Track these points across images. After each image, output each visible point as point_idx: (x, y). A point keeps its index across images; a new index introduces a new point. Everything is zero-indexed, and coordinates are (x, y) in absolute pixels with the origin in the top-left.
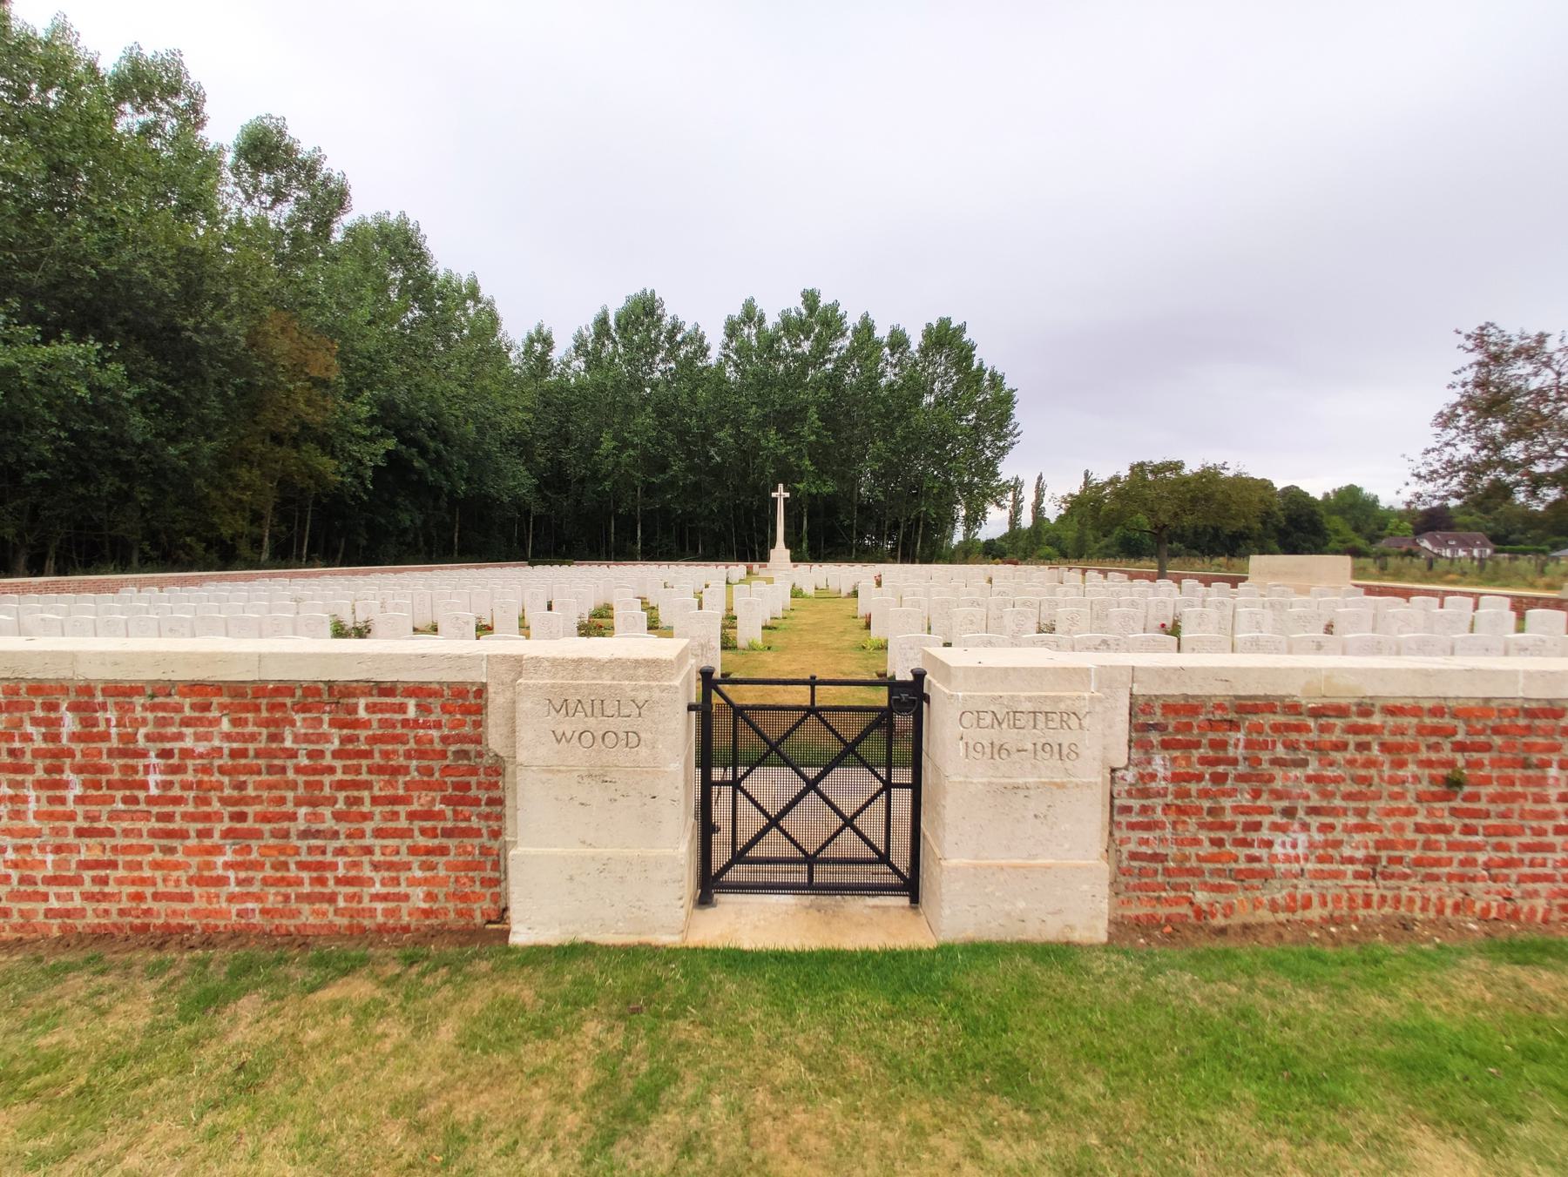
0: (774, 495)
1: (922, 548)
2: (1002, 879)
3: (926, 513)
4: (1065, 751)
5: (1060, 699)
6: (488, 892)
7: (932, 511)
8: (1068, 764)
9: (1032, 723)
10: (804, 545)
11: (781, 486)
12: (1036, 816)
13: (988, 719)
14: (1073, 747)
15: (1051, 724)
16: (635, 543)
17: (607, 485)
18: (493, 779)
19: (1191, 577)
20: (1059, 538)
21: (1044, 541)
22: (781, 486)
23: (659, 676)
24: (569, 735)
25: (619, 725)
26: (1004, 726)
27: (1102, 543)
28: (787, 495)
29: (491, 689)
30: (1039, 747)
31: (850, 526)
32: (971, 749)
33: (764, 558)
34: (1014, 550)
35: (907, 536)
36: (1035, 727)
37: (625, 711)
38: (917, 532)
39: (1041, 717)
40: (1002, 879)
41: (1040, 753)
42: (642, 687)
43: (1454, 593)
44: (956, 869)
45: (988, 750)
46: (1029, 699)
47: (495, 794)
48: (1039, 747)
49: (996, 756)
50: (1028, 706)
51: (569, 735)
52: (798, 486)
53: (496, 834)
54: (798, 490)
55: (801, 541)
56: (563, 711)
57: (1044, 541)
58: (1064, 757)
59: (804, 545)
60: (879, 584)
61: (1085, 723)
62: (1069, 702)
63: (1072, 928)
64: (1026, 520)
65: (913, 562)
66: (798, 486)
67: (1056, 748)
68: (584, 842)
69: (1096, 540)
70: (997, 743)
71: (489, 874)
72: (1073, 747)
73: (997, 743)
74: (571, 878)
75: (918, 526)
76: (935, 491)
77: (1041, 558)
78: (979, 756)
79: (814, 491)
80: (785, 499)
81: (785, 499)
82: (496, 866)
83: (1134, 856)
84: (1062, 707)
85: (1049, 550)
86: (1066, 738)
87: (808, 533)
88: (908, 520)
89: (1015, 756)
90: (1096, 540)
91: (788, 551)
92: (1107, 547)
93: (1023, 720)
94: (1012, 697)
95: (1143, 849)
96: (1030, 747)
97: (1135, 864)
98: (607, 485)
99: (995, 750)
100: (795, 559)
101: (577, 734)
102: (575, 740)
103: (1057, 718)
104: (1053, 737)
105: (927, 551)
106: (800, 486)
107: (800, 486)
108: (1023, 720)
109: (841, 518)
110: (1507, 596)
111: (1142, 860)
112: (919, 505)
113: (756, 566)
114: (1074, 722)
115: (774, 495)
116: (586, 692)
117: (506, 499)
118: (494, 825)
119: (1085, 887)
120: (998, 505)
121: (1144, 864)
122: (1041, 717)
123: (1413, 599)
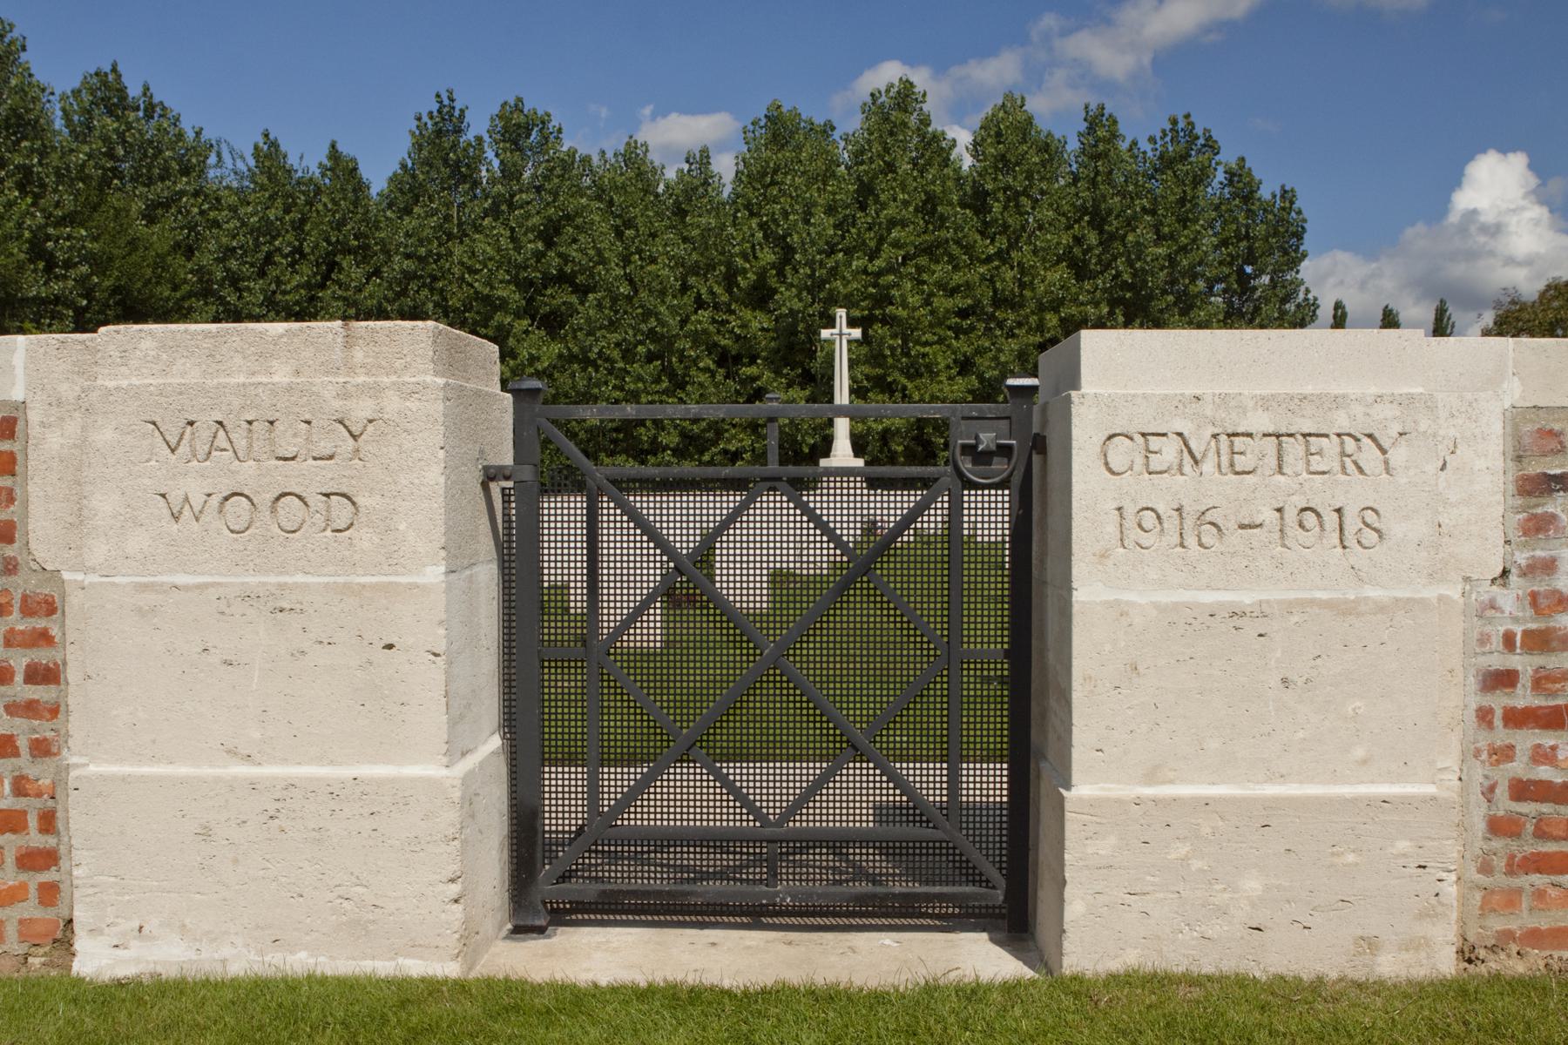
2: (1206, 830)
4: (1352, 524)
5: (1338, 401)
6: (34, 880)
8: (1357, 555)
9: (1272, 461)
12: (1284, 681)
13: (1169, 451)
14: (1370, 517)
15: (1317, 463)
18: (40, 623)
23: (398, 364)
24: (197, 500)
25: (310, 477)
26: (1208, 466)
29: (34, 416)
30: (1291, 515)
32: (1131, 522)
36: (1280, 470)
37: (325, 447)
39: (1294, 449)
40: (1206, 830)
41: (1293, 531)
42: (363, 389)
44: (1094, 804)
45: (1171, 524)
46: (1265, 403)
47: (43, 656)
48: (1291, 515)
49: (1191, 541)
50: (1260, 422)
51: (197, 500)
53: (42, 749)
56: (184, 449)
58: (1350, 540)
60: (1261, 635)
61: (1398, 456)
62: (1358, 410)
63: (1370, 944)
67: (1331, 519)
68: (232, 752)
70: (1191, 510)
71: (35, 839)
72: (1370, 517)
73: (1191, 510)
74: (205, 833)
78: (1146, 540)
82: (48, 822)
83: (1521, 790)
84: (1342, 422)
86: (1353, 494)
89: (1236, 538)
93: (1256, 453)
94: (1224, 398)
95: (1544, 773)
96: (1269, 516)
97: (1528, 808)
99: (1189, 523)
101: (215, 501)
102: (210, 516)
103: (1330, 446)
104: (1323, 495)
108: (1256, 453)
111: (1542, 800)
114: (1369, 456)
116: (236, 403)
118: (44, 729)
119: (1403, 845)
121: (1546, 808)
122: (1294, 449)
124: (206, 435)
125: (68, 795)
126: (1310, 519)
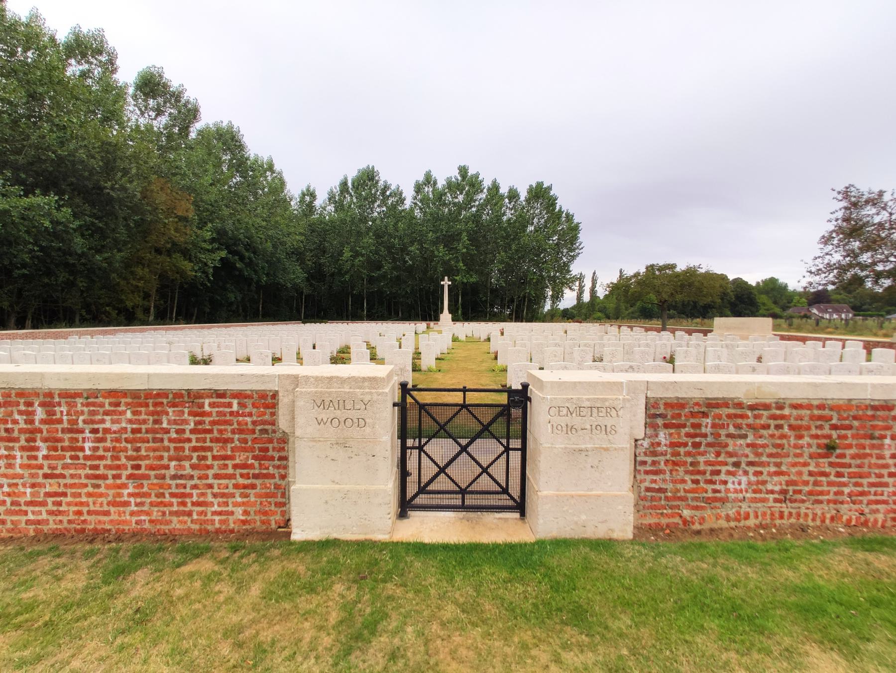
0: (442, 283)
1: (527, 313)
2: (572, 503)
3: (529, 293)
4: (609, 429)
5: (606, 400)
7: (532, 292)
8: (611, 437)
9: (590, 414)
10: (460, 312)
11: (446, 278)
12: (592, 467)
13: (565, 411)
14: (613, 427)
15: (601, 414)
16: (363, 311)
17: (347, 277)
18: (282, 446)
19: (681, 330)
20: (605, 308)
21: (597, 309)
22: (446, 278)
23: (377, 386)
24: (325, 420)
25: (354, 414)
26: (574, 415)
27: (630, 311)
28: (450, 283)
29: (280, 394)
30: (594, 427)
31: (486, 301)
32: (555, 428)
33: (437, 319)
34: (580, 315)
35: (518, 306)
36: (591, 416)
37: (357, 407)
38: (524, 304)
39: (595, 410)
40: (572, 503)
41: (594, 430)
42: (367, 393)
43: (831, 339)
45: (565, 429)
46: (588, 400)
47: (283, 454)
48: (594, 427)
49: (569, 432)
50: (587, 404)
51: (325, 420)
52: (456, 278)
53: (283, 477)
54: (456, 280)
55: (458, 309)
56: (322, 407)
57: (597, 309)
58: (608, 433)
59: (460, 312)
60: (502, 334)
61: (620, 413)
62: (611, 402)
63: (612, 530)
64: (586, 297)
65: (522, 321)
66: (456, 278)
67: (603, 428)
68: (333, 482)
69: (626, 309)
70: (570, 425)
71: (279, 500)
72: (613, 427)
73: (570, 425)
74: (326, 502)
75: (524, 301)
76: (534, 281)
77: (595, 319)
79: (465, 281)
80: (449, 285)
81: (449, 285)
82: (283, 495)
83: (648, 489)
84: (607, 404)
85: (599, 314)
86: (609, 422)
87: (462, 305)
88: (519, 297)
89: (580, 432)
90: (626, 309)
91: (450, 315)
92: (633, 313)
93: (585, 412)
94: (579, 398)
95: (653, 485)
96: (588, 427)
97: (648, 494)
98: (347, 277)
99: (569, 429)
100: (455, 320)
101: (330, 420)
102: (328, 423)
103: (604, 410)
104: (602, 421)
105: (530, 315)
106: (457, 278)
107: (457, 278)
108: (585, 412)
109: (481, 296)
110: (861, 341)
111: (652, 492)
112: (525, 289)
113: (432, 324)
114: (613, 413)
115: (442, 283)
116: (335, 396)
117: (289, 285)
118: (283, 472)
119: (620, 507)
120: (570, 288)
121: (654, 494)
122: (595, 410)
123: (808, 342)
124: (328, 403)
125: (561, 544)
126: (599, 428)
